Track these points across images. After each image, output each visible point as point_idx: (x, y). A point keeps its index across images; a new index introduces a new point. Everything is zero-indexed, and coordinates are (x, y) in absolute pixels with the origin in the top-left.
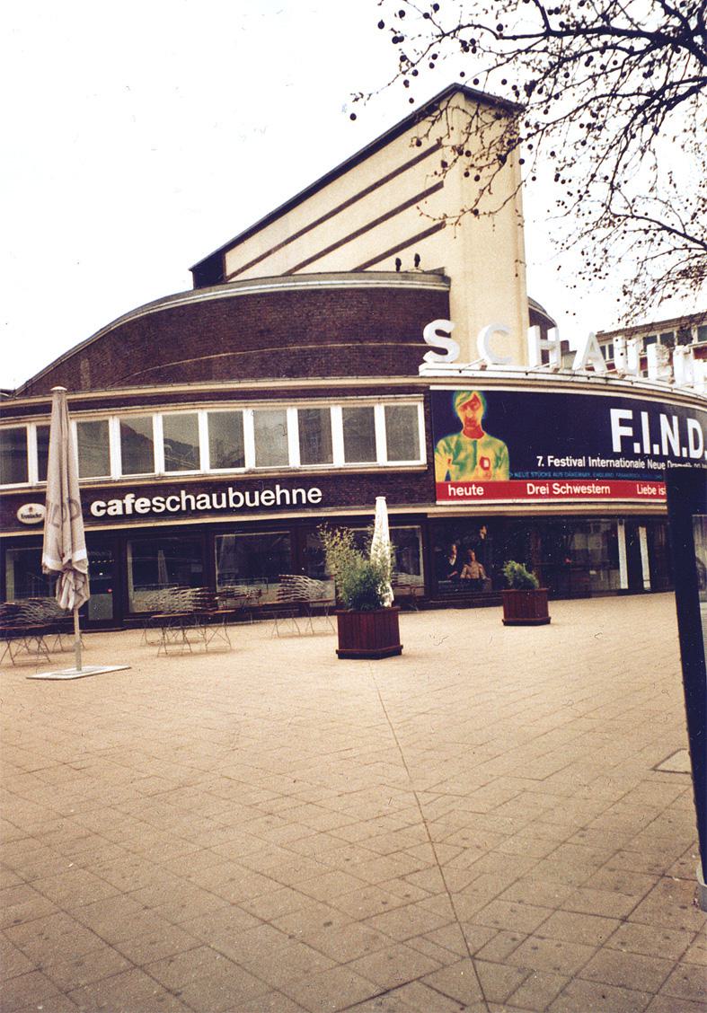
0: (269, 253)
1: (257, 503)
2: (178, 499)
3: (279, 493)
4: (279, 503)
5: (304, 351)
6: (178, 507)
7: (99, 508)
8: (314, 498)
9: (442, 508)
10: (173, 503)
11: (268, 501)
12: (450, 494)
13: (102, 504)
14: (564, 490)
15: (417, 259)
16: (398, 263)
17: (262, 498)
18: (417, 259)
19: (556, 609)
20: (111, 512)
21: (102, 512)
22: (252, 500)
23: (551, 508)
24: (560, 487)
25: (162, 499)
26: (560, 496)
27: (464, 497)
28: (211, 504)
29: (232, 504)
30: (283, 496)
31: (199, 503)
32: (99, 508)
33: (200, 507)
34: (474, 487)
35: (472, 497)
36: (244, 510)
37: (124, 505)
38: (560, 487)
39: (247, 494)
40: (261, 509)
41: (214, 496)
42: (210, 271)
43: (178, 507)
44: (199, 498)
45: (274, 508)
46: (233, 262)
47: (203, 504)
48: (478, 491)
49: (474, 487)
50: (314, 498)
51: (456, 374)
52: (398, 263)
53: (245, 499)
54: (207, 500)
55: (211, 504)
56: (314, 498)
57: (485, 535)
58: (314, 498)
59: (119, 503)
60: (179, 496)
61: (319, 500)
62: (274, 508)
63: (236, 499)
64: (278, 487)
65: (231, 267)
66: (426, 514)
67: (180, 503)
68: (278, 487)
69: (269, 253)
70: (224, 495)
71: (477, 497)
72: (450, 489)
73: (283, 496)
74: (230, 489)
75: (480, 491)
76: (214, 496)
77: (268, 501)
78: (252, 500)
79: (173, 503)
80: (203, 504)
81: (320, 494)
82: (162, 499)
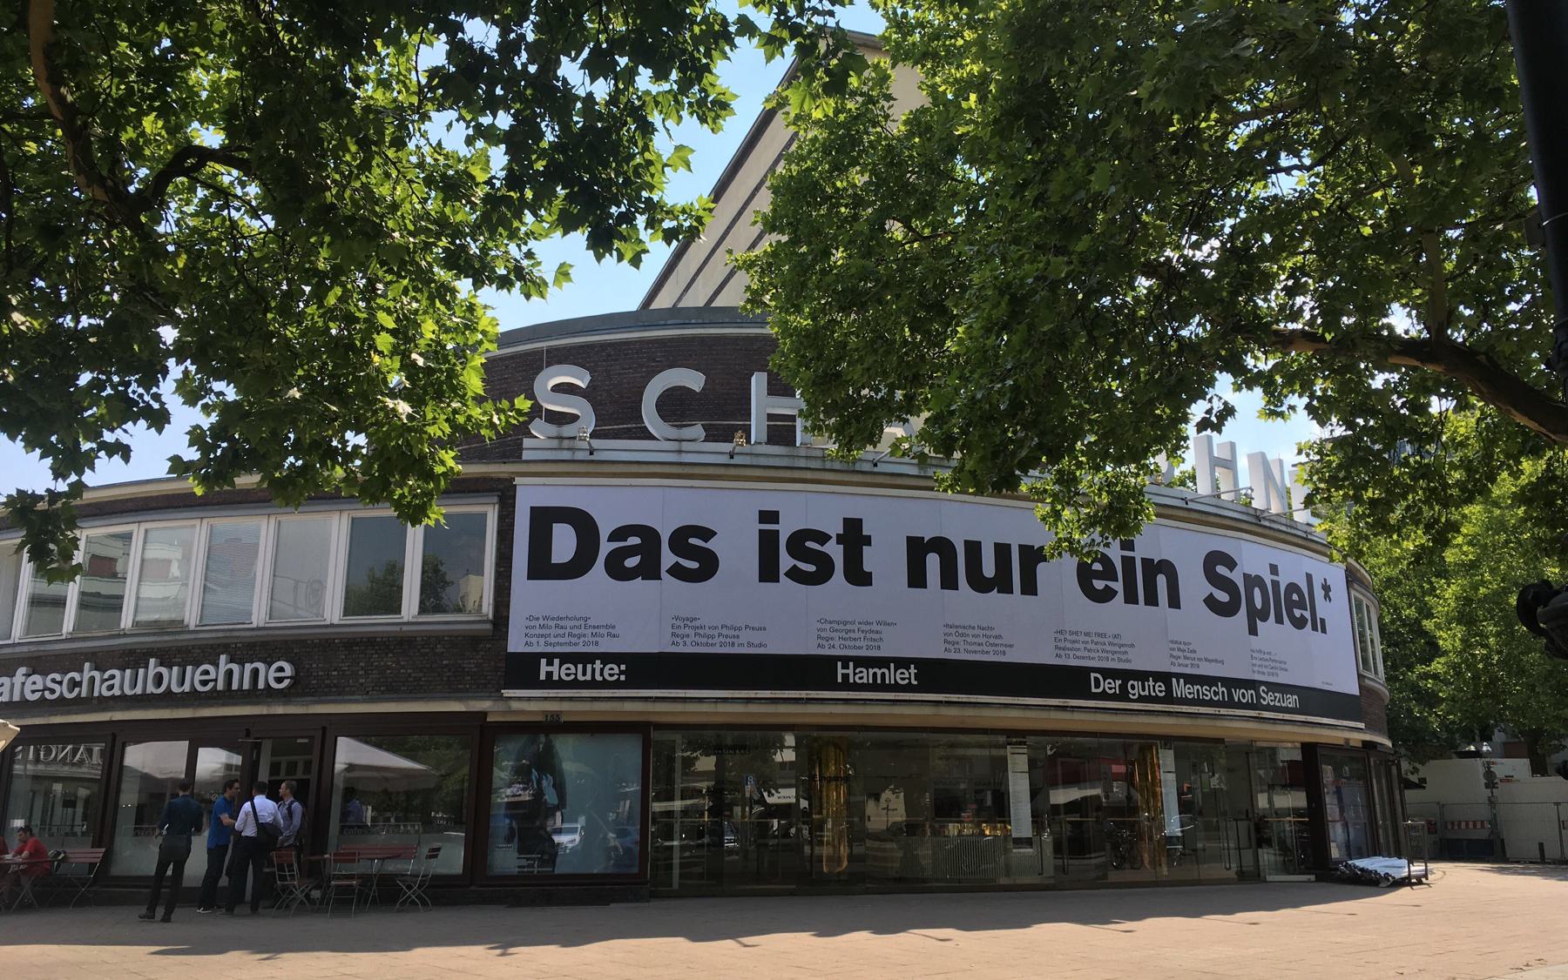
1: (588, 677)
3: (223, 667)
4: (220, 687)
6: (211, 685)
9: (524, 702)
10: (74, 684)
14: (1216, 693)
21: (37, 696)
23: (1077, 716)
27: (575, 684)
28: (122, 688)
29: (151, 689)
30: (230, 673)
36: (168, 699)
37: (13, 685)
40: (193, 698)
43: (211, 685)
44: (106, 676)
45: (214, 697)
53: (171, 676)
54: (117, 682)
55: (122, 688)
56: (279, 680)
60: (81, 671)
61: (286, 683)
62: (214, 697)
63: (159, 679)
66: (484, 714)
72: (840, 671)
73: (230, 673)
74: (152, 661)
75: (1292, 701)
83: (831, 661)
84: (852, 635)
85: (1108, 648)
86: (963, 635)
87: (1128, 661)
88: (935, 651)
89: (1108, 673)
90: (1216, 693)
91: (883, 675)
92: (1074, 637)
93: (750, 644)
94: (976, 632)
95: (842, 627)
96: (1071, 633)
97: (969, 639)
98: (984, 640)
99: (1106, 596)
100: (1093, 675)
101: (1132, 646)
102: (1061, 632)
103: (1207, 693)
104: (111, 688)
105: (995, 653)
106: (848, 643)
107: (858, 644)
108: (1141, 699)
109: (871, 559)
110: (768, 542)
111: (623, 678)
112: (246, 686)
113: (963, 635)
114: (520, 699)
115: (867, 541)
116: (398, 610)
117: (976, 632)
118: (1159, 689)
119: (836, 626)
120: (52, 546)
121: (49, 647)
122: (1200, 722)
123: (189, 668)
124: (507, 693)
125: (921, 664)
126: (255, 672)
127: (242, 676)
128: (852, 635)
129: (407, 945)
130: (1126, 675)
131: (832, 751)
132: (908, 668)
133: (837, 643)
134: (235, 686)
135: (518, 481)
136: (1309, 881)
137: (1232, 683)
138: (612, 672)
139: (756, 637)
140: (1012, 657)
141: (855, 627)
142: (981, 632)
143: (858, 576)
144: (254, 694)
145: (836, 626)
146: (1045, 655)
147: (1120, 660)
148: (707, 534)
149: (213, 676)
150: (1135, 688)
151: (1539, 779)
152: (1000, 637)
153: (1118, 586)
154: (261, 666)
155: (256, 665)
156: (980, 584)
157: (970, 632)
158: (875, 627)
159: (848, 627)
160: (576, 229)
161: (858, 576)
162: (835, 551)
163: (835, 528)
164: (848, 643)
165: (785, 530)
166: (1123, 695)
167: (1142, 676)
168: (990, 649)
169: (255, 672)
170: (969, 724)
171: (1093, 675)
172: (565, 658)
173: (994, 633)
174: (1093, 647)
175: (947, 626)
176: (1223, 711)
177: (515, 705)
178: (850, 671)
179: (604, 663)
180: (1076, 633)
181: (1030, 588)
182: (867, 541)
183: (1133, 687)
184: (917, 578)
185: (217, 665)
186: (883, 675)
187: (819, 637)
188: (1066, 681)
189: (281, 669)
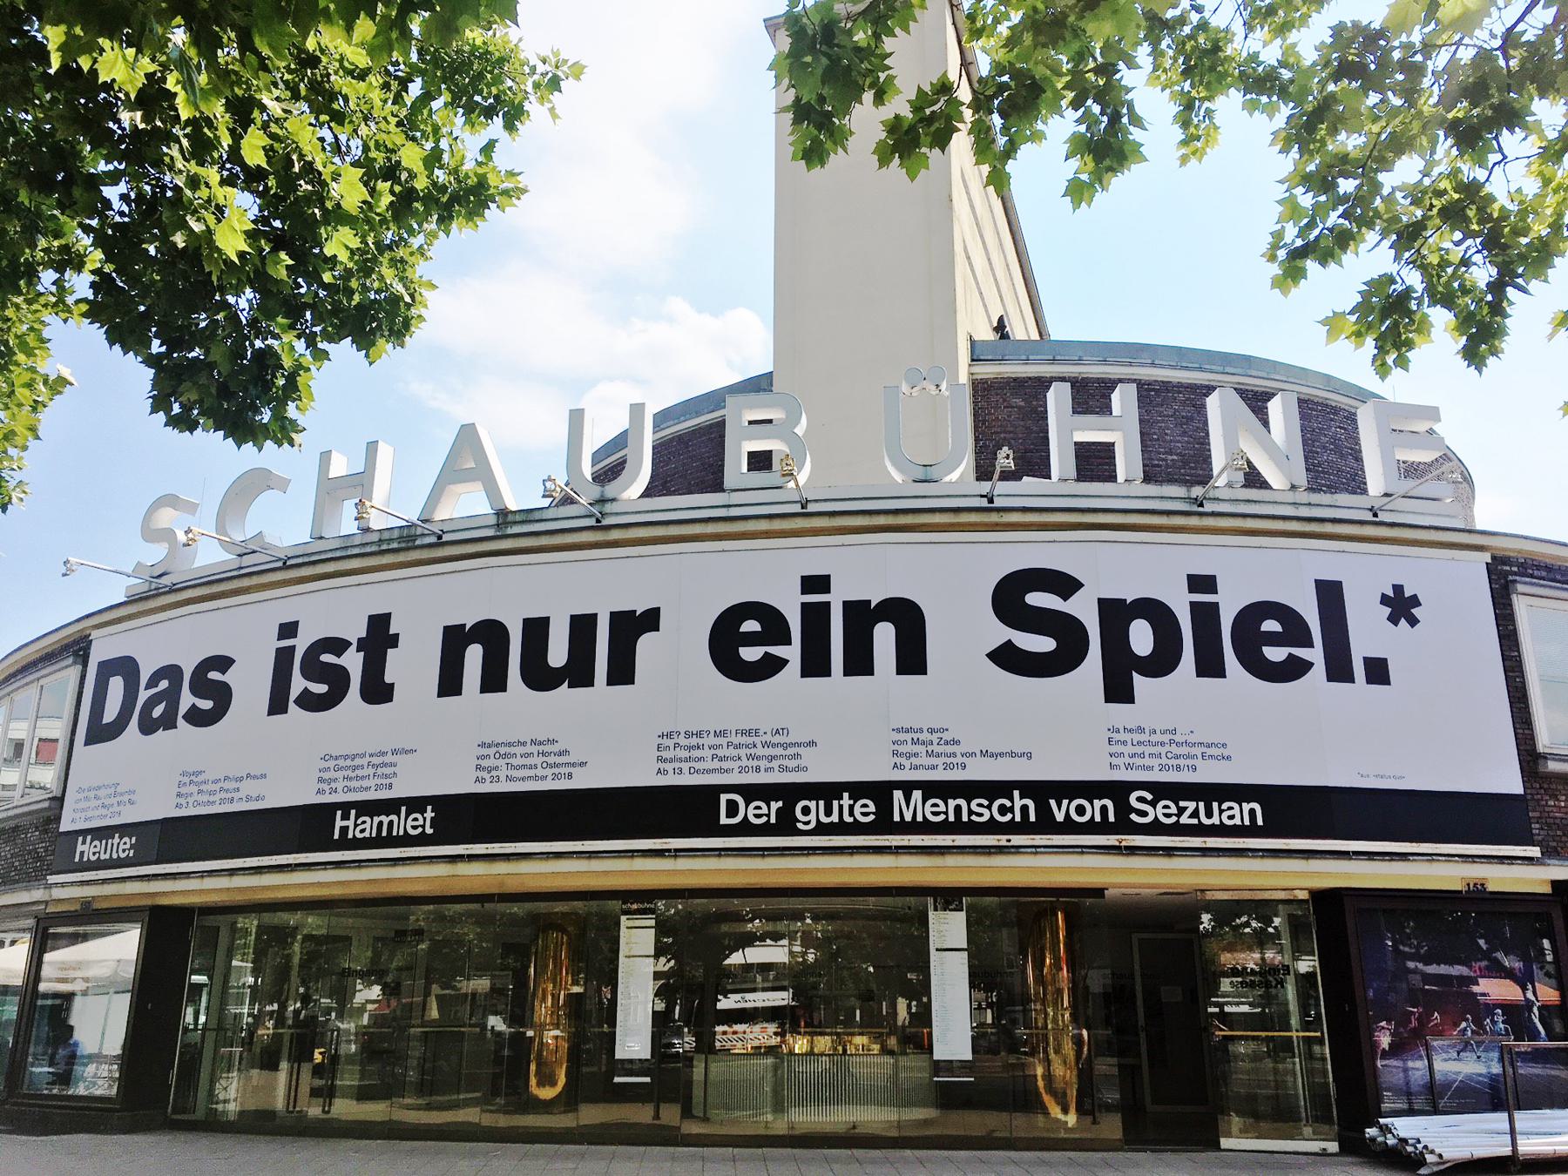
2: (1008, 804)
3: (1018, 803)
4: (952, 818)
6: (1009, 816)
8: (934, 814)
12: (897, 818)
14: (1003, 810)
19: (388, 680)
23: (683, 864)
24: (1153, 804)
25: (986, 803)
26: (1156, 828)
31: (1225, 815)
33: (359, 836)
34: (846, 800)
35: (841, 828)
38: (1153, 804)
41: (384, 834)
43: (1009, 816)
47: (1231, 817)
48: (858, 810)
49: (846, 800)
50: (934, 814)
57: (1373, 1139)
61: (872, 817)
67: (1011, 810)
70: (835, 803)
71: (857, 828)
72: (339, 823)
75: (123, 846)
76: (384, 834)
77: (936, 814)
80: (363, 831)
81: (872, 808)
83: (323, 814)
84: (359, 773)
85: (760, 751)
86: (505, 756)
87: (805, 769)
88: (460, 781)
89: (751, 792)
90: (1003, 810)
91: (391, 823)
92: (694, 741)
93: (249, 799)
94: (529, 749)
95: (349, 762)
96: (688, 735)
97: (514, 761)
98: (538, 760)
99: (1294, 670)
100: (724, 798)
101: (812, 743)
102: (669, 735)
103: (981, 809)
104: (363, 831)
105: (556, 777)
106: (354, 784)
107: (365, 783)
108: (821, 829)
109: (395, 667)
110: (283, 659)
111: (429, 831)
113: (505, 756)
114: (63, 885)
115: (394, 641)
117: (529, 749)
118: (865, 810)
119: (341, 763)
122: (951, 860)
124: (52, 879)
125: (439, 802)
128: (359, 773)
129: (463, 1123)
130: (791, 793)
132: (423, 812)
133: (340, 785)
136: (1324, 1153)
137: (1041, 791)
138: (123, 846)
139: (248, 787)
140: (582, 780)
141: (364, 762)
142: (534, 749)
143: (378, 691)
145: (341, 763)
146: (641, 773)
147: (783, 769)
148: (1006, 657)
150: (811, 813)
152: (957, 742)
153: (1315, 654)
154: (962, 802)
156: (540, 677)
157: (519, 750)
158: (389, 758)
159: (358, 762)
161: (378, 691)
162: (353, 662)
163: (355, 630)
164: (354, 784)
165: (301, 643)
166: (785, 824)
167: (827, 792)
168: (549, 772)
170: (512, 886)
171: (724, 798)
172: (933, 789)
173: (555, 748)
174: (732, 752)
175: (483, 745)
176: (1017, 840)
177: (58, 893)
178: (350, 823)
179: (855, 797)
180: (699, 734)
181: (622, 672)
182: (394, 641)
183: (806, 811)
184: (450, 684)
186: (391, 823)
187: (478, 767)
188: (681, 811)
189: (865, 806)
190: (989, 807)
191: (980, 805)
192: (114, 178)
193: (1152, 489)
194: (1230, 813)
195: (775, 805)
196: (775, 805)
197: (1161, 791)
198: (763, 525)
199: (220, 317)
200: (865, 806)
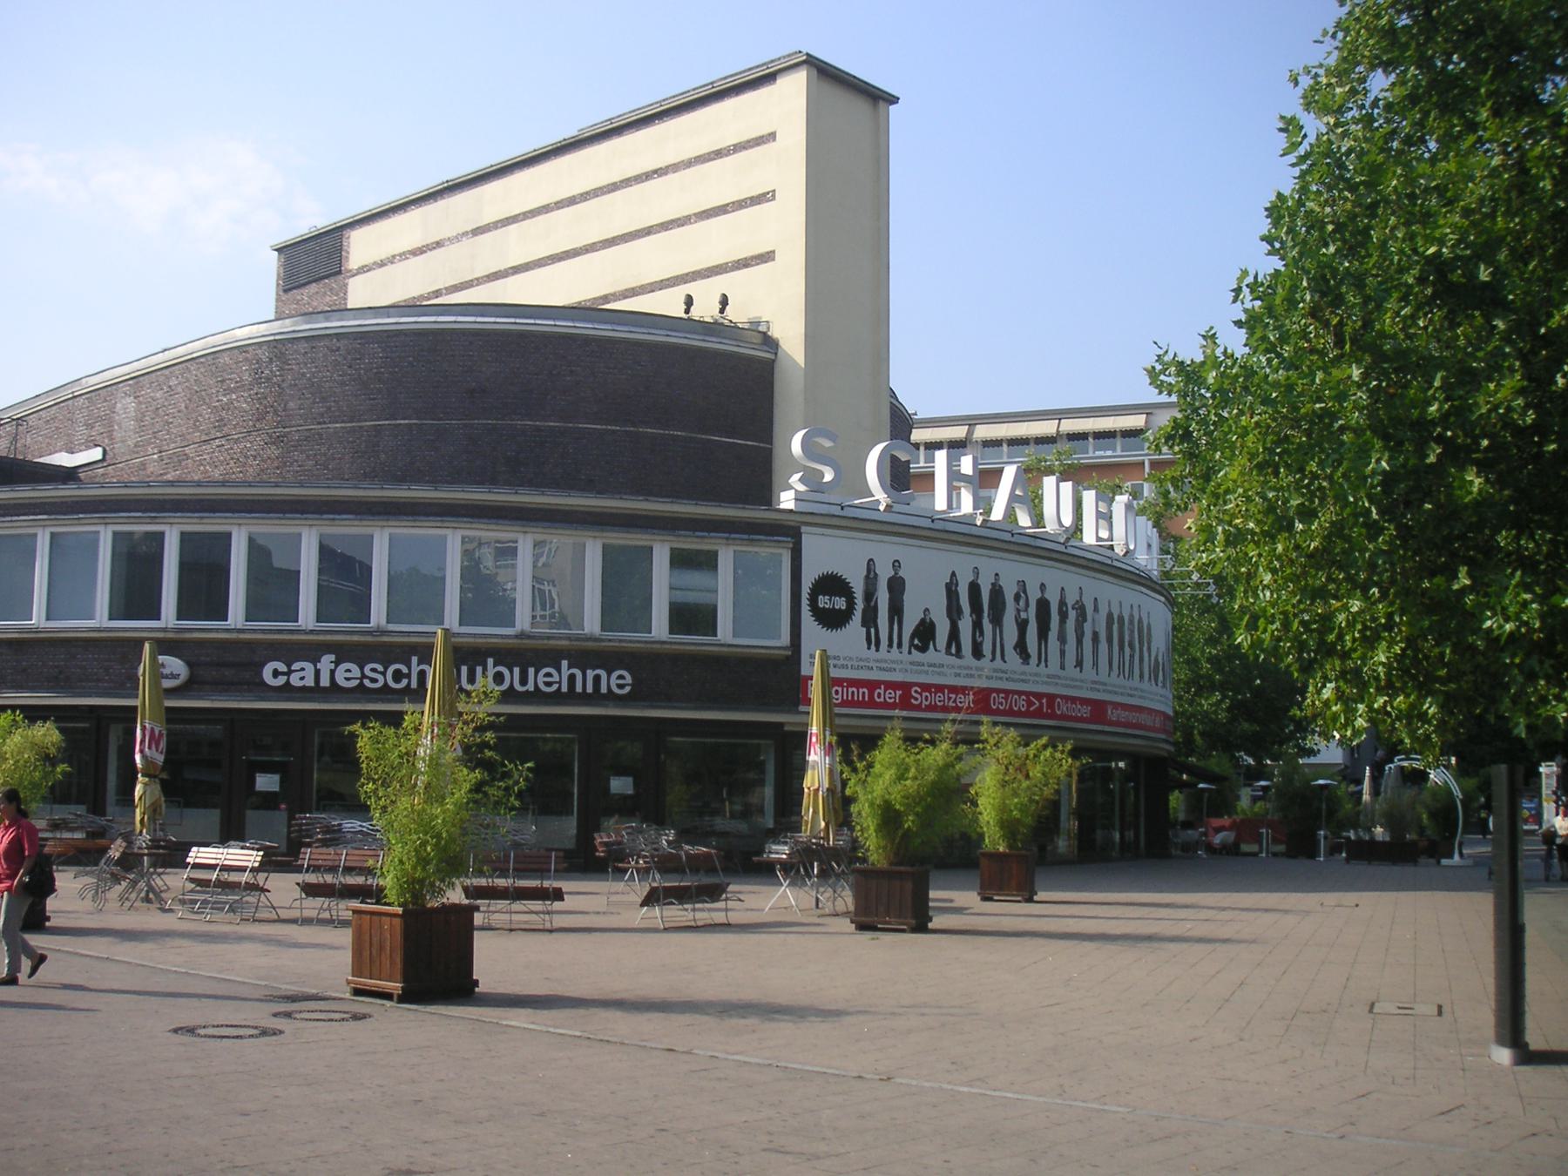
0: (439, 244)
2: (405, 670)
3: (566, 672)
4: (565, 689)
5: (538, 429)
6: (555, 687)
7: (276, 673)
11: (548, 684)
13: (282, 667)
15: (724, 302)
16: (689, 301)
17: (539, 679)
18: (724, 302)
20: (295, 680)
21: (281, 680)
22: (524, 682)
23: (1131, 741)
25: (380, 668)
30: (572, 678)
32: (276, 673)
37: (317, 673)
39: (517, 670)
40: (537, 696)
41: (464, 669)
42: (313, 260)
43: (405, 682)
45: (557, 698)
46: (361, 247)
49: (327, 662)
51: (836, 510)
52: (689, 301)
56: (621, 686)
58: (621, 686)
59: (309, 666)
61: (628, 689)
62: (571, 697)
64: (565, 663)
65: (355, 258)
66: (781, 725)
67: (408, 676)
68: (565, 663)
69: (439, 244)
73: (572, 678)
74: (490, 661)
77: (548, 684)
78: (524, 682)
79: (398, 676)
81: (629, 679)
82: (282, 667)
112: (590, 690)
116: (115, 534)
120: (1487, 532)
121: (188, 635)
123: (531, 671)
126: (597, 679)
127: (585, 680)
131: (994, 840)
134: (579, 689)
135: (803, 529)
144: (596, 697)
149: (556, 678)
151: (269, 266)
155: (598, 671)
160: (53, 880)
169: (597, 679)
185: (559, 671)
189: (621, 677)
190: (384, 674)
191: (373, 670)
192: (1464, 591)
193: (705, 546)
194: (302, 674)
195: (899, 693)
196: (899, 693)
197: (926, 687)
198: (961, 539)
199: (1502, 256)
200: (621, 677)
